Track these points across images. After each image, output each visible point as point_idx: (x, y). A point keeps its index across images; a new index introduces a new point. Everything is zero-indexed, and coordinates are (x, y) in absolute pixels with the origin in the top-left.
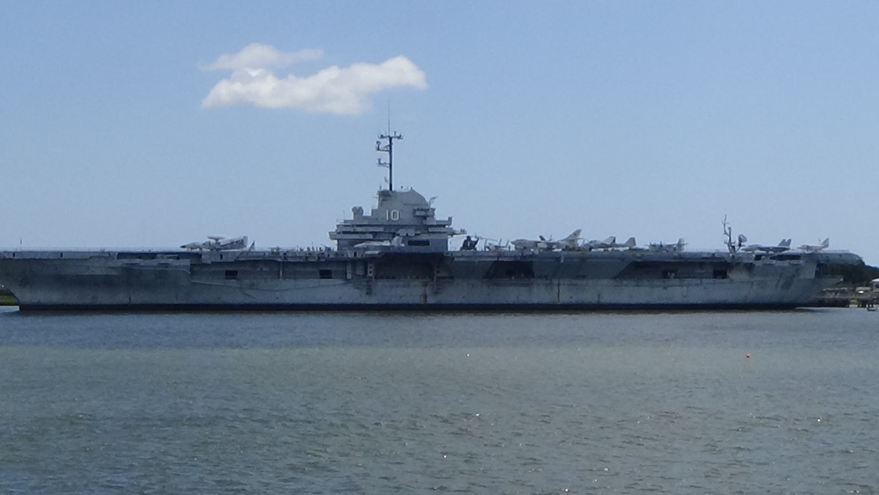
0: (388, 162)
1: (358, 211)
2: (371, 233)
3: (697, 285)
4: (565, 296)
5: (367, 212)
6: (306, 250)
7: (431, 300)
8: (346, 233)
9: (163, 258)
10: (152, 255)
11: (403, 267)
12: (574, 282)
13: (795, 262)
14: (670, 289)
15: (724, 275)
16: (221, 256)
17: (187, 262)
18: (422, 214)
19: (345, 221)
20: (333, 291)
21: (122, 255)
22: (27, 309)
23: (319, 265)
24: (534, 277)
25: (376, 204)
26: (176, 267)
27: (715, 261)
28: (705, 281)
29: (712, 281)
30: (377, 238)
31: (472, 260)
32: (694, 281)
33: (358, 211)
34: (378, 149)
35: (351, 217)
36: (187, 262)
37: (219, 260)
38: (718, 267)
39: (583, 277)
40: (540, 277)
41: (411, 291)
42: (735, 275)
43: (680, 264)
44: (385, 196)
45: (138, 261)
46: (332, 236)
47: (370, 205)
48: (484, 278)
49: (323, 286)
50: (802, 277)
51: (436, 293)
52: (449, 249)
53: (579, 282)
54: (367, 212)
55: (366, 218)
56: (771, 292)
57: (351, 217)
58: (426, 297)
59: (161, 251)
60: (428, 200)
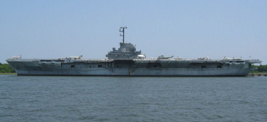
0: (123, 35)
1: (114, 49)
2: (117, 55)
3: (211, 70)
4: (172, 74)
5: (117, 49)
6: (206, 59)
7: (131, 74)
8: (109, 55)
9: (53, 61)
10: (50, 61)
11: (125, 63)
12: (175, 69)
13: (242, 63)
14: (204, 71)
15: (220, 67)
16: (70, 61)
17: (60, 63)
18: (133, 51)
19: (110, 52)
20: (102, 71)
21: (42, 61)
22: (19, 75)
23: (100, 64)
24: (162, 67)
25: (119, 47)
26: (56, 64)
27: (217, 63)
28: (215, 69)
29: (217, 69)
30: (119, 56)
31: (141, 62)
32: (211, 69)
33: (114, 49)
34: (120, 31)
35: (112, 50)
36: (60, 63)
37: (68, 62)
38: (219, 65)
39: (177, 67)
40: (164, 67)
41: (125, 71)
42: (224, 67)
43: (206, 63)
44: (122, 45)
45: (45, 62)
46: (107, 56)
47: (117, 47)
48: (147, 68)
49: (99, 70)
50: (244, 67)
51: (133, 72)
52: (247, 68)
53: (176, 69)
54: (117, 49)
55: (117, 51)
56: (234, 71)
57: (112, 50)
58: (130, 73)
59: (53, 59)
60: (134, 46)
